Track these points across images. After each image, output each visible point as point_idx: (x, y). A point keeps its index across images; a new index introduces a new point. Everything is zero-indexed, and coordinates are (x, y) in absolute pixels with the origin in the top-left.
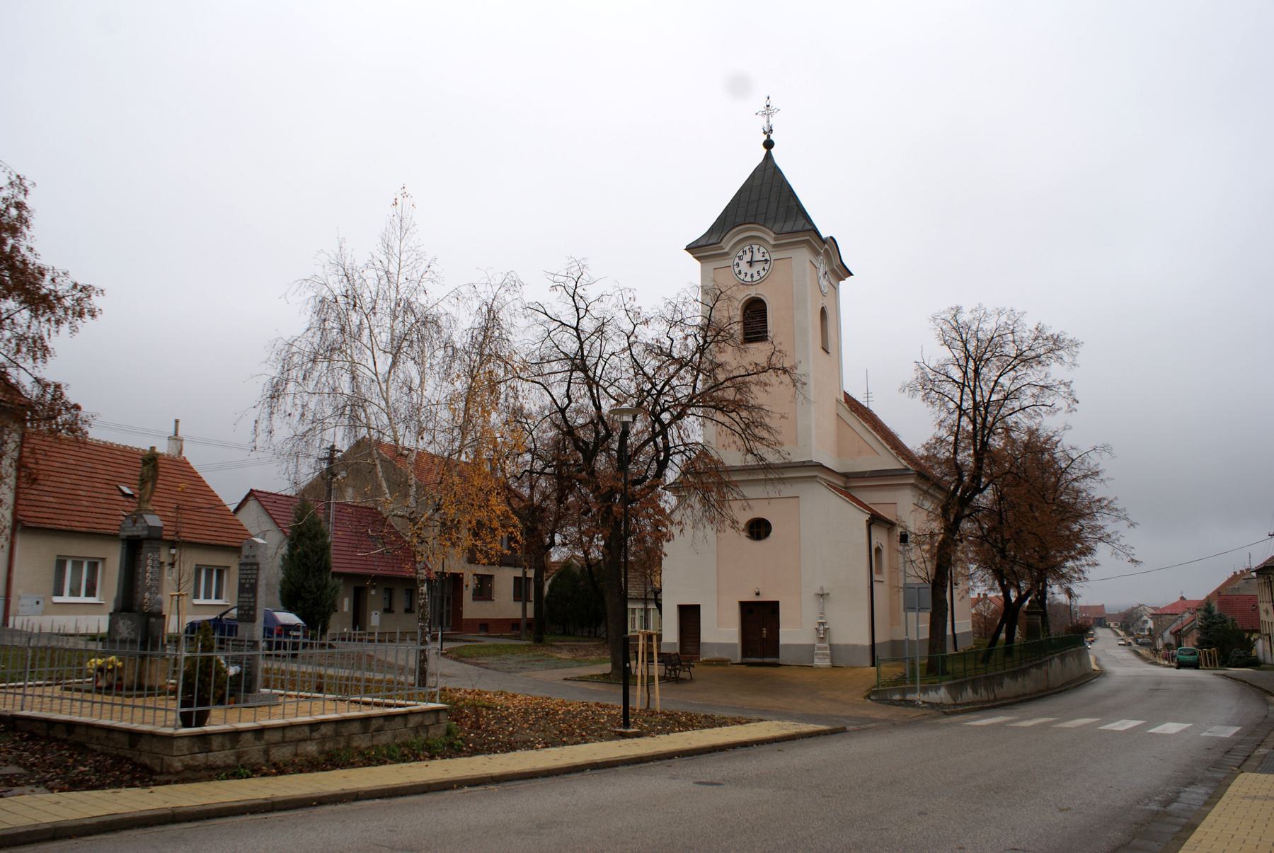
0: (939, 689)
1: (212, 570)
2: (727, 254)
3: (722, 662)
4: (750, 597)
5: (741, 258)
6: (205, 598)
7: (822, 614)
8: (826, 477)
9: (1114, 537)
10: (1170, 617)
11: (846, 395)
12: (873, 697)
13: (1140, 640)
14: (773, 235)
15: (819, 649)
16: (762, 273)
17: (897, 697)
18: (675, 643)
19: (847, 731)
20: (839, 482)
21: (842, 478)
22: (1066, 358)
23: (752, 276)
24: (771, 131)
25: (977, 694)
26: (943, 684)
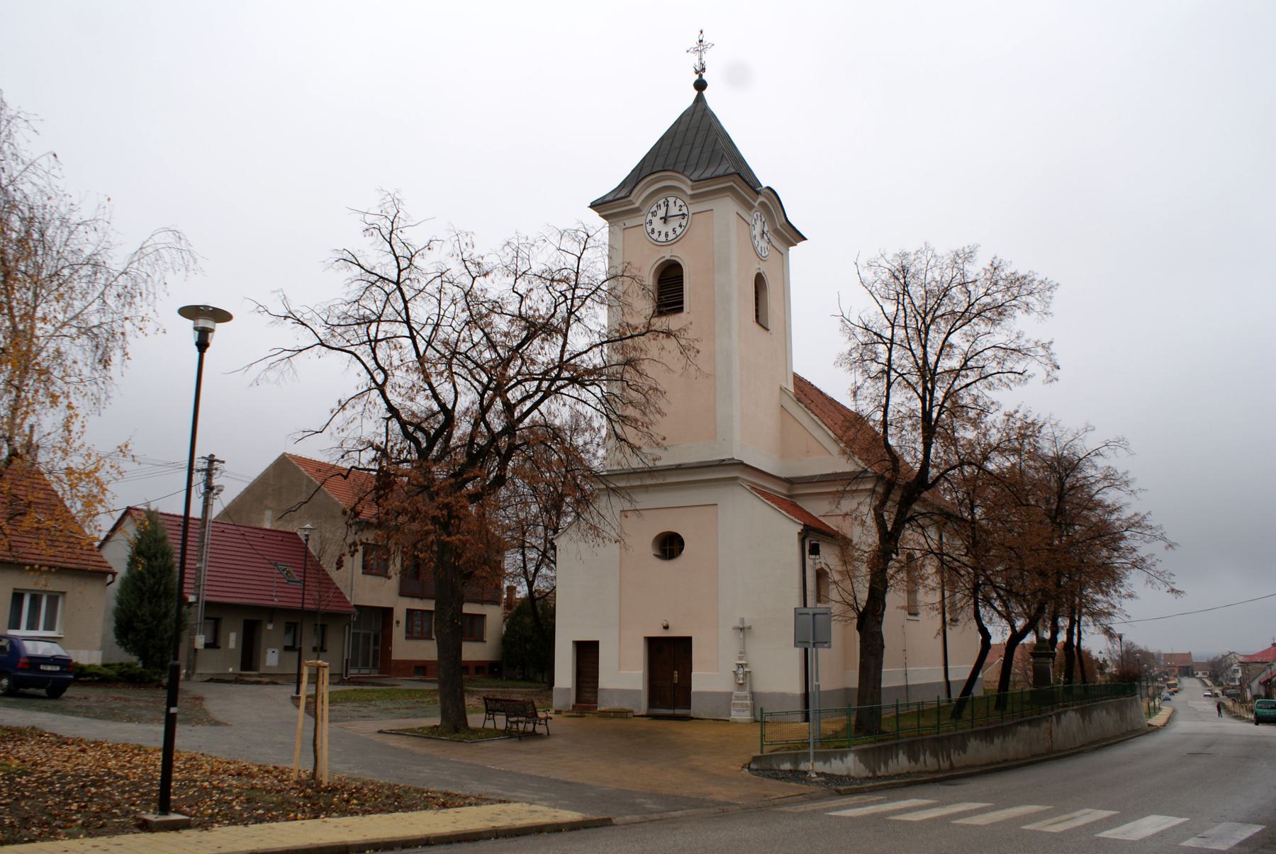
0: (846, 756)
1: (41, 596)
2: (637, 210)
3: (621, 714)
4: (658, 632)
5: (654, 214)
6: (45, 629)
7: (742, 654)
8: (752, 480)
9: (1149, 562)
10: (1259, 666)
11: (799, 381)
12: (753, 766)
13: (1228, 691)
14: (689, 183)
15: (738, 698)
16: (679, 231)
17: (787, 766)
18: (569, 689)
19: (612, 825)
20: (781, 490)
21: (785, 484)
22: (1038, 307)
23: (667, 235)
24: (704, 70)
25: (917, 761)
26: (853, 748)
